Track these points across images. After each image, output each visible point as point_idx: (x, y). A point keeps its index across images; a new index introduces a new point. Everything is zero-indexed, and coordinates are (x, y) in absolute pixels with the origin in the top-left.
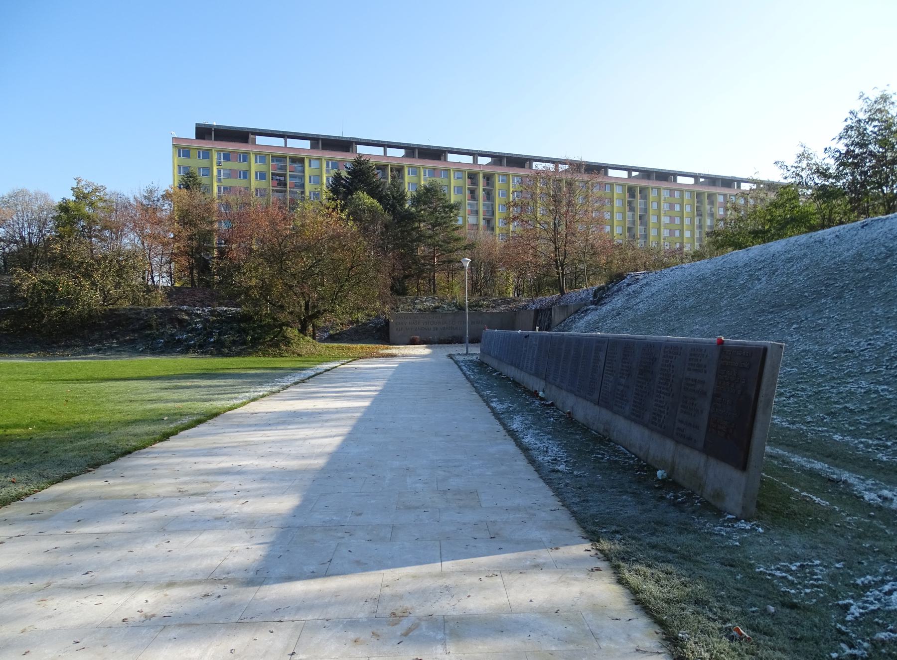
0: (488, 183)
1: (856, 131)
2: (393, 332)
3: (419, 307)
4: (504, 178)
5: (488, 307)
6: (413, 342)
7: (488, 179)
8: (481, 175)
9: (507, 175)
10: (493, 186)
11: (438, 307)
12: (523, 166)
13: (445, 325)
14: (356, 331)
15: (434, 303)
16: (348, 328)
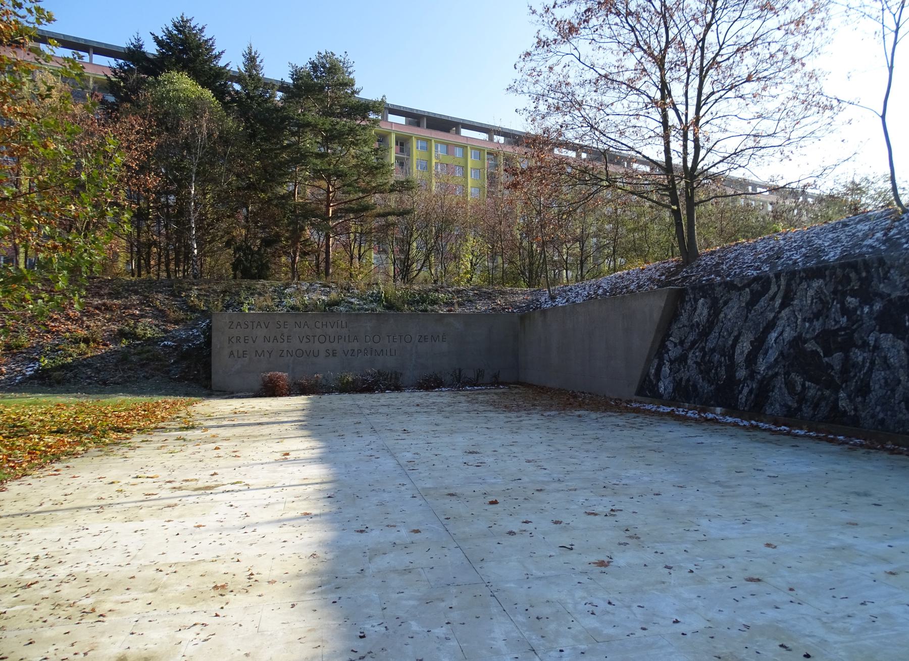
0: (402, 151)
1: (309, 600)
2: (223, 362)
3: (291, 302)
4: (424, 145)
5: (449, 304)
6: (270, 390)
7: (402, 144)
8: (393, 137)
9: (428, 141)
10: (409, 154)
11: (337, 303)
12: (447, 130)
13: (355, 345)
14: (123, 358)
15: (327, 294)
16: (103, 350)
